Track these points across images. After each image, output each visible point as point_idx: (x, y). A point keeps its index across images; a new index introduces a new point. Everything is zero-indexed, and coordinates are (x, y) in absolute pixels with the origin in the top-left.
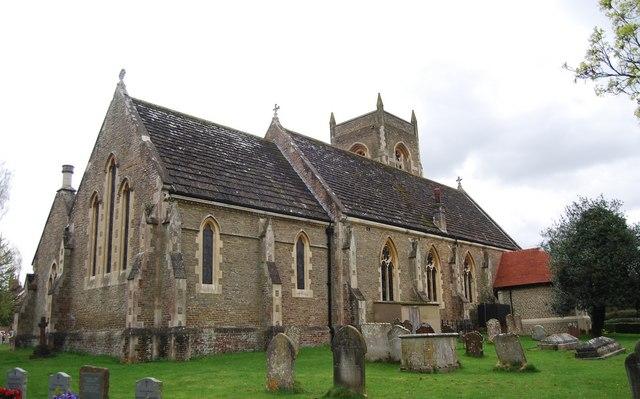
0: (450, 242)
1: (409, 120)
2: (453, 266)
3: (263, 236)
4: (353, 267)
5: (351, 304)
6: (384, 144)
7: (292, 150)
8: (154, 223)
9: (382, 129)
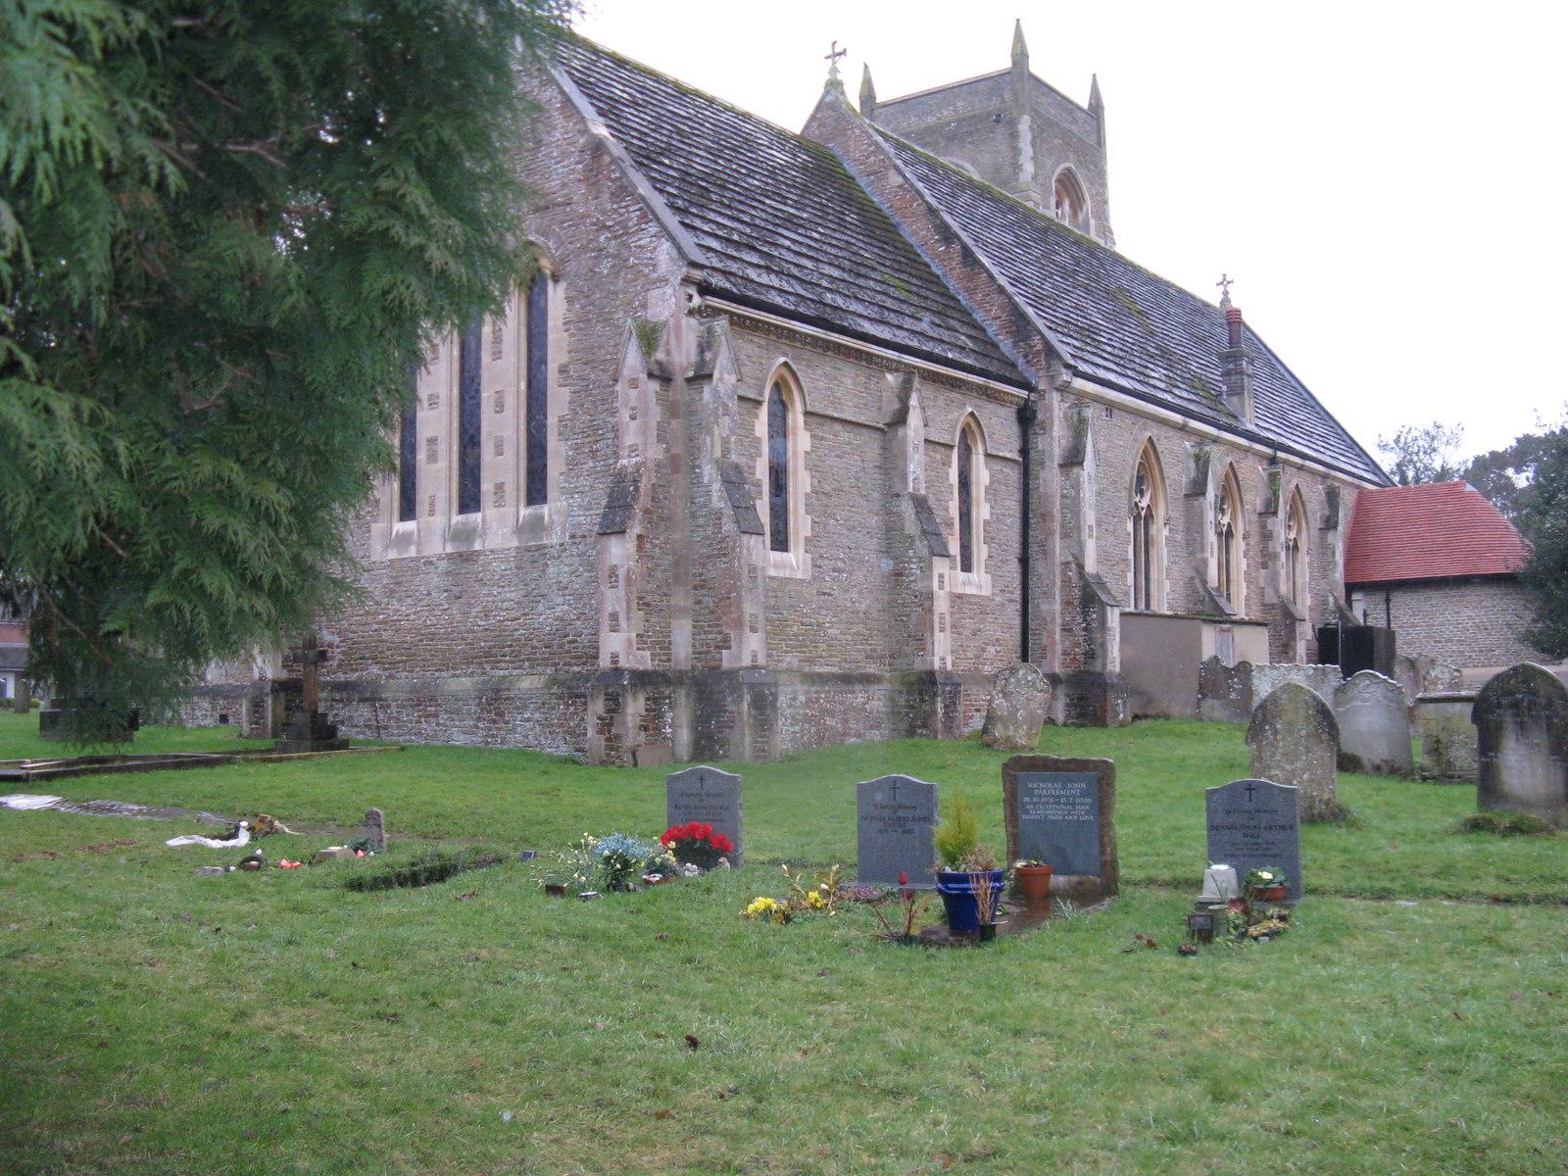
0: (1261, 456)
1: (1084, 103)
2: (1270, 521)
3: (900, 418)
4: (1089, 517)
5: (1085, 614)
6: (1029, 168)
7: (895, 180)
8: (663, 375)
9: (1024, 125)
